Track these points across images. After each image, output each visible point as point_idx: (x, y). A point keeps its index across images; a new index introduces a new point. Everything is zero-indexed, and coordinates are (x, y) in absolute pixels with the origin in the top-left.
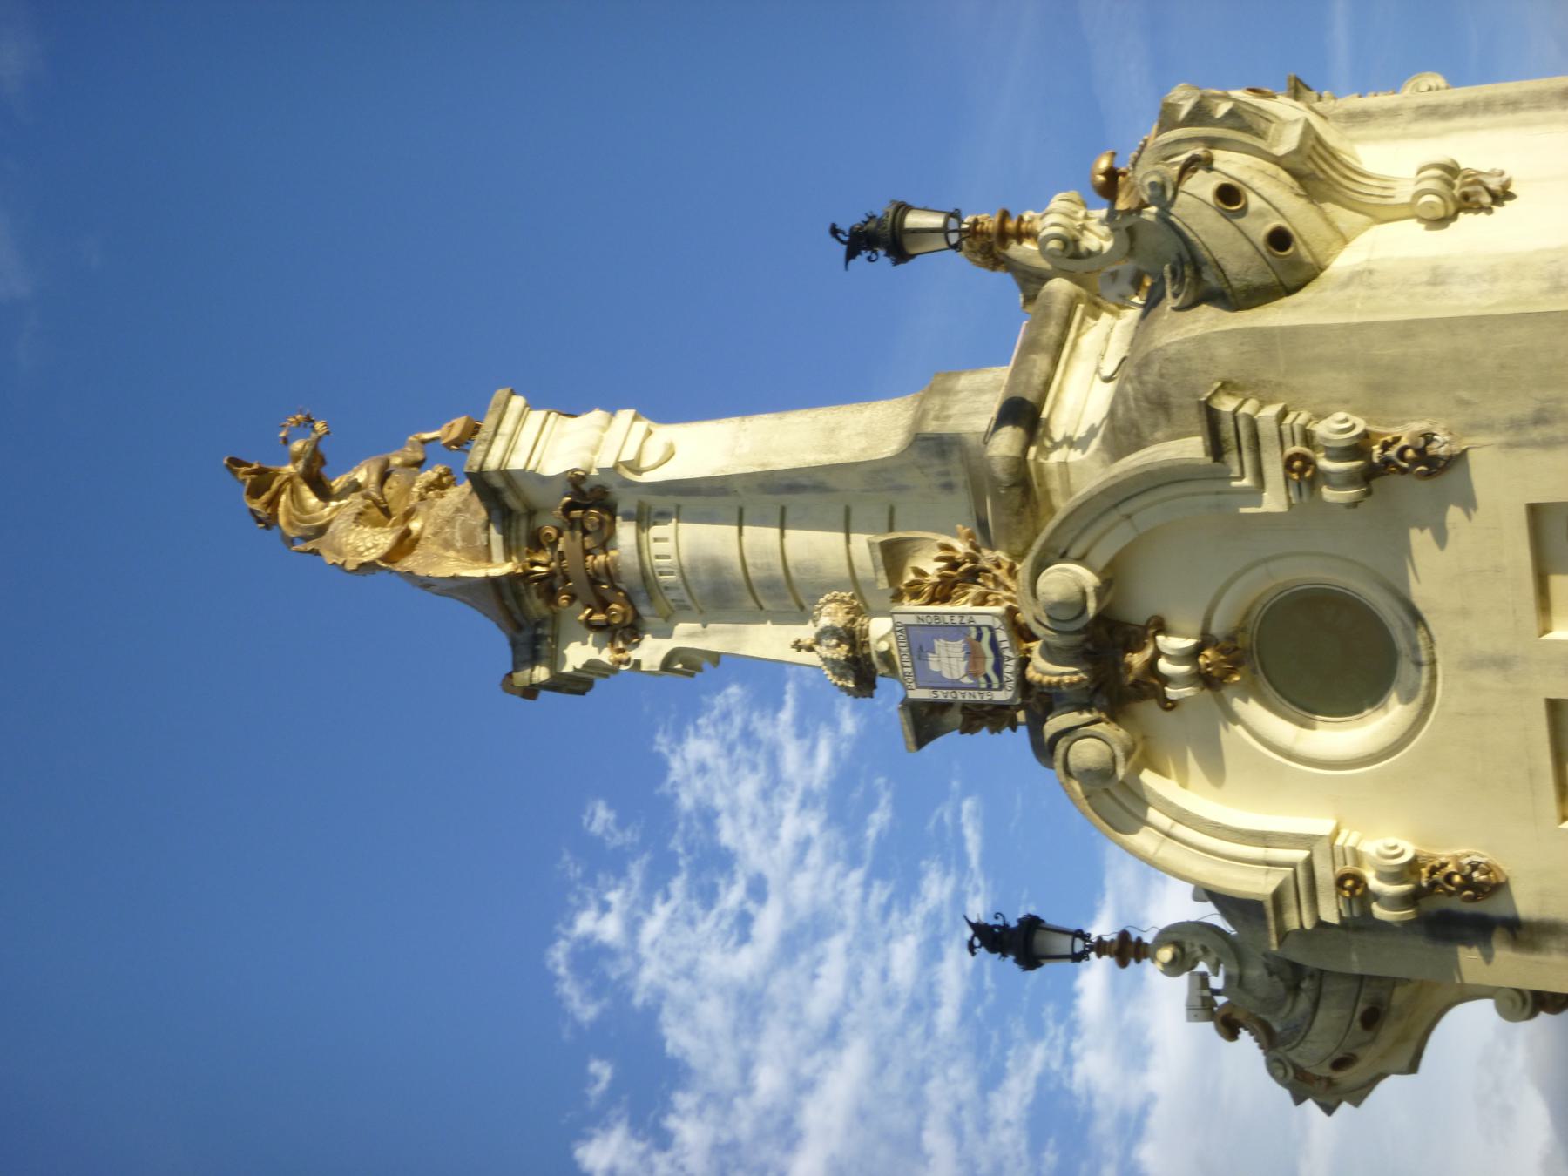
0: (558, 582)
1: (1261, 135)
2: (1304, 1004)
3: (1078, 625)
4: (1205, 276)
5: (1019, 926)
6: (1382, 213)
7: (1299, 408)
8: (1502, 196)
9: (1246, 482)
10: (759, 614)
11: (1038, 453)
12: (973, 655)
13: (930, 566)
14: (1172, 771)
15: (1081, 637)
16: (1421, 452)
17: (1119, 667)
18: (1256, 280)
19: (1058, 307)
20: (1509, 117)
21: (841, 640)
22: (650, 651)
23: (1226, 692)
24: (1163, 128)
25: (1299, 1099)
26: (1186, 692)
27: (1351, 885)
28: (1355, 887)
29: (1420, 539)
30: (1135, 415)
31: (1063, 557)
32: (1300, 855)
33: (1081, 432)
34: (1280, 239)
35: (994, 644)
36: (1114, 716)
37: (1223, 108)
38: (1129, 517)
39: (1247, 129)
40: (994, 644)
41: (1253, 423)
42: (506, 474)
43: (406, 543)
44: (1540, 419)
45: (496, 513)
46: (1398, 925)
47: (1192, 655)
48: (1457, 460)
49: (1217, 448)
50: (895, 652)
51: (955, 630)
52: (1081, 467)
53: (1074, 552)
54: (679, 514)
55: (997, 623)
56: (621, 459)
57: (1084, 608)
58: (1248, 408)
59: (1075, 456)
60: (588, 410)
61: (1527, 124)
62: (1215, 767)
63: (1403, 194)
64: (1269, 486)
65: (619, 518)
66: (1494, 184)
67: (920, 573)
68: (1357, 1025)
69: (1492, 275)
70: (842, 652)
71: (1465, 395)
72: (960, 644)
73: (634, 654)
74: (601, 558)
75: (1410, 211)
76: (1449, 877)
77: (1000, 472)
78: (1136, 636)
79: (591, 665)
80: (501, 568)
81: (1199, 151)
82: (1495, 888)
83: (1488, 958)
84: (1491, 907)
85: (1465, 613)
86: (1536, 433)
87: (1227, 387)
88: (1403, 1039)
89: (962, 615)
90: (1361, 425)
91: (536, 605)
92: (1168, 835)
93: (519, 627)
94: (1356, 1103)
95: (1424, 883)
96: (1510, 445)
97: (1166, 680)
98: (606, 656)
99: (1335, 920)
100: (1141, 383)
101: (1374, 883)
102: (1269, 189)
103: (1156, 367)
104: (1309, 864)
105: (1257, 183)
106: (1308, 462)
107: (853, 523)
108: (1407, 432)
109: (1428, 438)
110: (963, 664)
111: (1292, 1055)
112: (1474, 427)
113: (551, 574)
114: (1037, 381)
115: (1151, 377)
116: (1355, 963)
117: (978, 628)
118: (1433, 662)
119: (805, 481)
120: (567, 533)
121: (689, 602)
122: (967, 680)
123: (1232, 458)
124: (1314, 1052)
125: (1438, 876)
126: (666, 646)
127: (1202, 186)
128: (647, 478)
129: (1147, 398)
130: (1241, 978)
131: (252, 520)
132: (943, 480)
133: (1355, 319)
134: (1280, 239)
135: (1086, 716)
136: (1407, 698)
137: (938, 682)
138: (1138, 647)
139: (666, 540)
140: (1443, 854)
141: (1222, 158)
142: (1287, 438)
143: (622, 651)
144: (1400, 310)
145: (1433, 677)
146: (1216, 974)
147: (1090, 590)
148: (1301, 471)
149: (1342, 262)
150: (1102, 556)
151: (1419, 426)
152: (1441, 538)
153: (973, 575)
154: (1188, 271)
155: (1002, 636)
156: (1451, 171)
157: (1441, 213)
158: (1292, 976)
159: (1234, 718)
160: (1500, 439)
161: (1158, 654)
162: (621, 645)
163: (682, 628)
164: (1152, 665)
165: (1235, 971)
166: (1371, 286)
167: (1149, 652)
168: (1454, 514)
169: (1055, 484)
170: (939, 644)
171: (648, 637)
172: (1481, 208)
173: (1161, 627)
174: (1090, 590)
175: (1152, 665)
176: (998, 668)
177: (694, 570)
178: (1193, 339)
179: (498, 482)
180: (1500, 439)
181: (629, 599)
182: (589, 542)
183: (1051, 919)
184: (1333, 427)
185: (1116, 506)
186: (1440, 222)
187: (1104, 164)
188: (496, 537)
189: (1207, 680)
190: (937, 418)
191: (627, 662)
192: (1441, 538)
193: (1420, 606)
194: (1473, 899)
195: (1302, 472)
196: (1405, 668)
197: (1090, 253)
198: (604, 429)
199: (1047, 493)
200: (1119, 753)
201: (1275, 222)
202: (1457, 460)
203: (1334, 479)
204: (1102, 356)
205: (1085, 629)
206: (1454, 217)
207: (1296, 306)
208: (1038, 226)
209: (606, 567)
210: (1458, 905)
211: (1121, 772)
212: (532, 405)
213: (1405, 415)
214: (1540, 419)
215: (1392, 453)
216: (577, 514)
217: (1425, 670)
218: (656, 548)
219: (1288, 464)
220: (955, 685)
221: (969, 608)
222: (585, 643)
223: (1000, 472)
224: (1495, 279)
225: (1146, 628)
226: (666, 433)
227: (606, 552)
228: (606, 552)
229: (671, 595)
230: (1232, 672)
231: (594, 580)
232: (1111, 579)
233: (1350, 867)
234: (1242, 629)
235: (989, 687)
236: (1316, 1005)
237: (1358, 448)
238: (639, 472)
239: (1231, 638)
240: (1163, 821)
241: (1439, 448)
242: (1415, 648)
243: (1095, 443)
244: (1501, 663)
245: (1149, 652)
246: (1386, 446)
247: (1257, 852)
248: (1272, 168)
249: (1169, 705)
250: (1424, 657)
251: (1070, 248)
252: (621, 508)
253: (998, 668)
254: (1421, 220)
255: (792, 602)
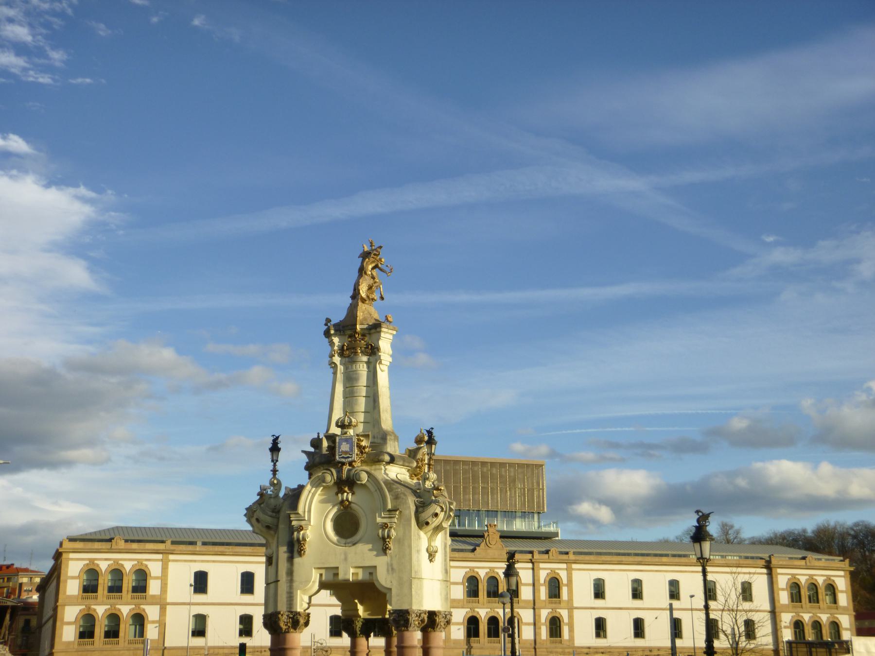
0: (353, 339)
1: (446, 520)
2: (270, 513)
3: (355, 479)
4: (421, 508)
5: (278, 447)
6: (430, 540)
7: (396, 525)
8: (431, 561)
9: (383, 515)
10: (345, 387)
11: (384, 464)
12: (346, 452)
13: (363, 444)
14: (322, 493)
15: (352, 478)
16: (387, 548)
17: (345, 485)
18: (420, 519)
19: (411, 465)
20: (443, 560)
21: (349, 423)
22: (337, 359)
23: (339, 505)
24: (449, 502)
25: (247, 509)
26: (340, 499)
27: (300, 528)
28: (300, 529)
29: (370, 546)
30: (394, 491)
31: (368, 477)
32: (306, 519)
33: (387, 472)
34: (427, 523)
35: (348, 457)
36: (335, 483)
37: (451, 514)
38: (376, 490)
39: (447, 518)
40: (348, 457)
41: (394, 517)
42: (380, 332)
43: (363, 301)
44: (392, 569)
45: (370, 326)
46: (293, 536)
47: (347, 500)
48: (386, 554)
49: (390, 511)
50: (346, 435)
51: (351, 449)
52: (381, 473)
53: (369, 479)
54: (369, 371)
55: (353, 459)
56: (382, 361)
57: (358, 481)
58: (397, 516)
59: (383, 472)
60: (392, 350)
61: (442, 563)
62: (323, 502)
63: (433, 544)
64: (382, 519)
65: (368, 357)
66: (433, 560)
67: (363, 441)
68: (267, 524)
69: (418, 561)
70: (346, 423)
71: (397, 556)
72: (348, 450)
73: (336, 355)
74: (359, 351)
75: (430, 545)
76: (302, 547)
77: (381, 457)
78: (351, 489)
79: (334, 343)
80: (358, 327)
81: (444, 510)
82: (300, 555)
83: (285, 552)
84: (296, 554)
85: (356, 553)
86: (390, 569)
87: (401, 512)
88: (261, 531)
89: (355, 451)
90: (393, 538)
91: (349, 332)
92: (310, 492)
93: (343, 327)
94: (247, 521)
95: (302, 542)
96: (388, 563)
97: (342, 494)
98: (336, 348)
99: (292, 524)
100: (401, 493)
101: (302, 533)
102: (436, 522)
103: (404, 497)
104: (305, 520)
105: (438, 520)
106: (387, 527)
107: (366, 413)
108: (391, 545)
109: (390, 549)
110: (344, 450)
111: (258, 510)
112: (391, 557)
113: (356, 338)
114: (398, 463)
115: (402, 495)
116: (281, 526)
117: (352, 454)
118: (346, 546)
119: (376, 404)
120: (365, 343)
121: (349, 370)
122: (341, 450)
123: (388, 513)
124: (259, 514)
125: (302, 545)
126: (338, 364)
127: (438, 510)
128: (378, 365)
129: (398, 494)
130: (271, 498)
131: (420, 430)
132: (376, 437)
133: (412, 537)
134: (427, 523)
135: (335, 478)
136: (338, 541)
137: (340, 444)
138: (349, 489)
139: (363, 368)
140: (306, 546)
141: (443, 513)
142: (391, 524)
143: (337, 352)
144: (413, 545)
145: (343, 546)
146: (271, 491)
147: (362, 482)
148: (385, 526)
149: (422, 533)
150: (368, 485)
151: (392, 548)
152: (370, 550)
153: (362, 453)
154: (422, 505)
155: (350, 459)
156: (436, 552)
157: (429, 551)
158: (276, 511)
159: (334, 506)
160: (389, 562)
161: (348, 493)
162: (338, 352)
163: (342, 367)
164: (345, 492)
165: (273, 496)
166: (418, 539)
167: (348, 491)
168: (375, 553)
169: (377, 467)
170: (348, 445)
171: (340, 359)
172: (429, 557)
173: (353, 494)
174: (362, 482)
175: (345, 492)
176: (343, 457)
177: (356, 374)
178: (410, 506)
179: (378, 330)
180: (389, 562)
181: (349, 356)
182: (363, 349)
183: (280, 453)
184: (393, 533)
185: (378, 489)
186: (427, 550)
187: (442, 488)
188: (365, 326)
189: (342, 502)
190: (390, 438)
191: (334, 353)
192: (370, 550)
193: (357, 545)
194: (298, 551)
195: (385, 526)
196: (343, 541)
197: (425, 482)
198: (388, 354)
199: (375, 465)
200: (328, 484)
201: (430, 523)
202: (386, 554)
203: (383, 532)
204: (401, 474)
205: (353, 480)
206: (428, 553)
207: (415, 525)
208: (431, 472)
209: (357, 352)
210: (296, 549)
211: (324, 484)
212: (394, 335)
213: (394, 545)
214: (392, 569)
215: (387, 543)
216: (370, 347)
217: (344, 545)
218: (361, 365)
219: (386, 524)
220: (339, 448)
221: (356, 452)
222: (339, 342)
223: (381, 457)
224: (418, 561)
225: (352, 491)
226: (385, 368)
227: (361, 352)
228: (361, 352)
229: (350, 367)
230: (343, 507)
231: (355, 348)
232: (364, 486)
233: (304, 528)
234: (351, 509)
235: (339, 455)
236: (271, 516)
237: (389, 537)
238: (379, 364)
239: (350, 507)
240: (312, 491)
241: (388, 551)
242: (348, 543)
243: (385, 476)
244: (346, 559)
245: (348, 491)
246: (389, 542)
247: (307, 510)
248: (440, 522)
249: (337, 494)
250: (347, 545)
251: (425, 479)
252: (371, 357)
253: (343, 457)
254: (428, 547)
255: (348, 396)
